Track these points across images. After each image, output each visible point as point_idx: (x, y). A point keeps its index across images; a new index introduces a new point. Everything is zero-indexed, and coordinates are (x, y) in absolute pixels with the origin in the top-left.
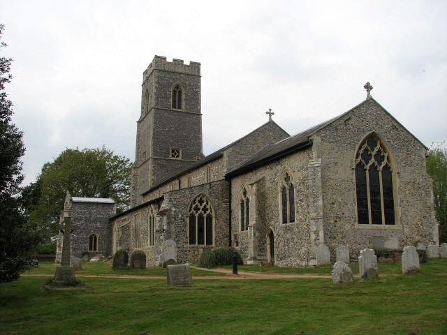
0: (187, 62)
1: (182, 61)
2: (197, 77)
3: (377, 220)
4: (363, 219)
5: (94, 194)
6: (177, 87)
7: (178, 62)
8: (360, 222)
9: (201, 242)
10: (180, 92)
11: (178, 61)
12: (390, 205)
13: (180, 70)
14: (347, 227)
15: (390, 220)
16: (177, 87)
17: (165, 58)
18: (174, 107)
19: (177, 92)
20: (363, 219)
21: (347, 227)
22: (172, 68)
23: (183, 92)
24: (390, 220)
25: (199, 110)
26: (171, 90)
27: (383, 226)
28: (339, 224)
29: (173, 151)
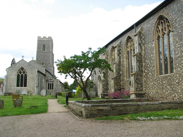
0: (42, 37)
1: (46, 37)
2: (52, 41)
3: (22, 86)
4: (18, 86)
5: (70, 72)
6: (44, 45)
7: (45, 37)
8: (17, 87)
9: (51, 89)
10: (45, 46)
11: (49, 37)
12: (26, 83)
13: (45, 40)
14: (13, 88)
15: (25, 86)
16: (44, 45)
17: (40, 37)
18: (43, 51)
19: (44, 46)
20: (18, 86)
21: (13, 88)
22: (42, 40)
23: (46, 46)
24: (25, 86)
25: (37, 53)
26: (42, 46)
27: (23, 87)
28: (11, 87)
29: (42, 63)
